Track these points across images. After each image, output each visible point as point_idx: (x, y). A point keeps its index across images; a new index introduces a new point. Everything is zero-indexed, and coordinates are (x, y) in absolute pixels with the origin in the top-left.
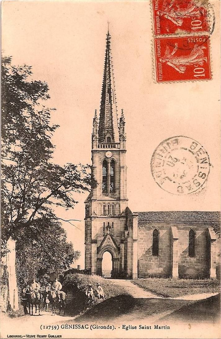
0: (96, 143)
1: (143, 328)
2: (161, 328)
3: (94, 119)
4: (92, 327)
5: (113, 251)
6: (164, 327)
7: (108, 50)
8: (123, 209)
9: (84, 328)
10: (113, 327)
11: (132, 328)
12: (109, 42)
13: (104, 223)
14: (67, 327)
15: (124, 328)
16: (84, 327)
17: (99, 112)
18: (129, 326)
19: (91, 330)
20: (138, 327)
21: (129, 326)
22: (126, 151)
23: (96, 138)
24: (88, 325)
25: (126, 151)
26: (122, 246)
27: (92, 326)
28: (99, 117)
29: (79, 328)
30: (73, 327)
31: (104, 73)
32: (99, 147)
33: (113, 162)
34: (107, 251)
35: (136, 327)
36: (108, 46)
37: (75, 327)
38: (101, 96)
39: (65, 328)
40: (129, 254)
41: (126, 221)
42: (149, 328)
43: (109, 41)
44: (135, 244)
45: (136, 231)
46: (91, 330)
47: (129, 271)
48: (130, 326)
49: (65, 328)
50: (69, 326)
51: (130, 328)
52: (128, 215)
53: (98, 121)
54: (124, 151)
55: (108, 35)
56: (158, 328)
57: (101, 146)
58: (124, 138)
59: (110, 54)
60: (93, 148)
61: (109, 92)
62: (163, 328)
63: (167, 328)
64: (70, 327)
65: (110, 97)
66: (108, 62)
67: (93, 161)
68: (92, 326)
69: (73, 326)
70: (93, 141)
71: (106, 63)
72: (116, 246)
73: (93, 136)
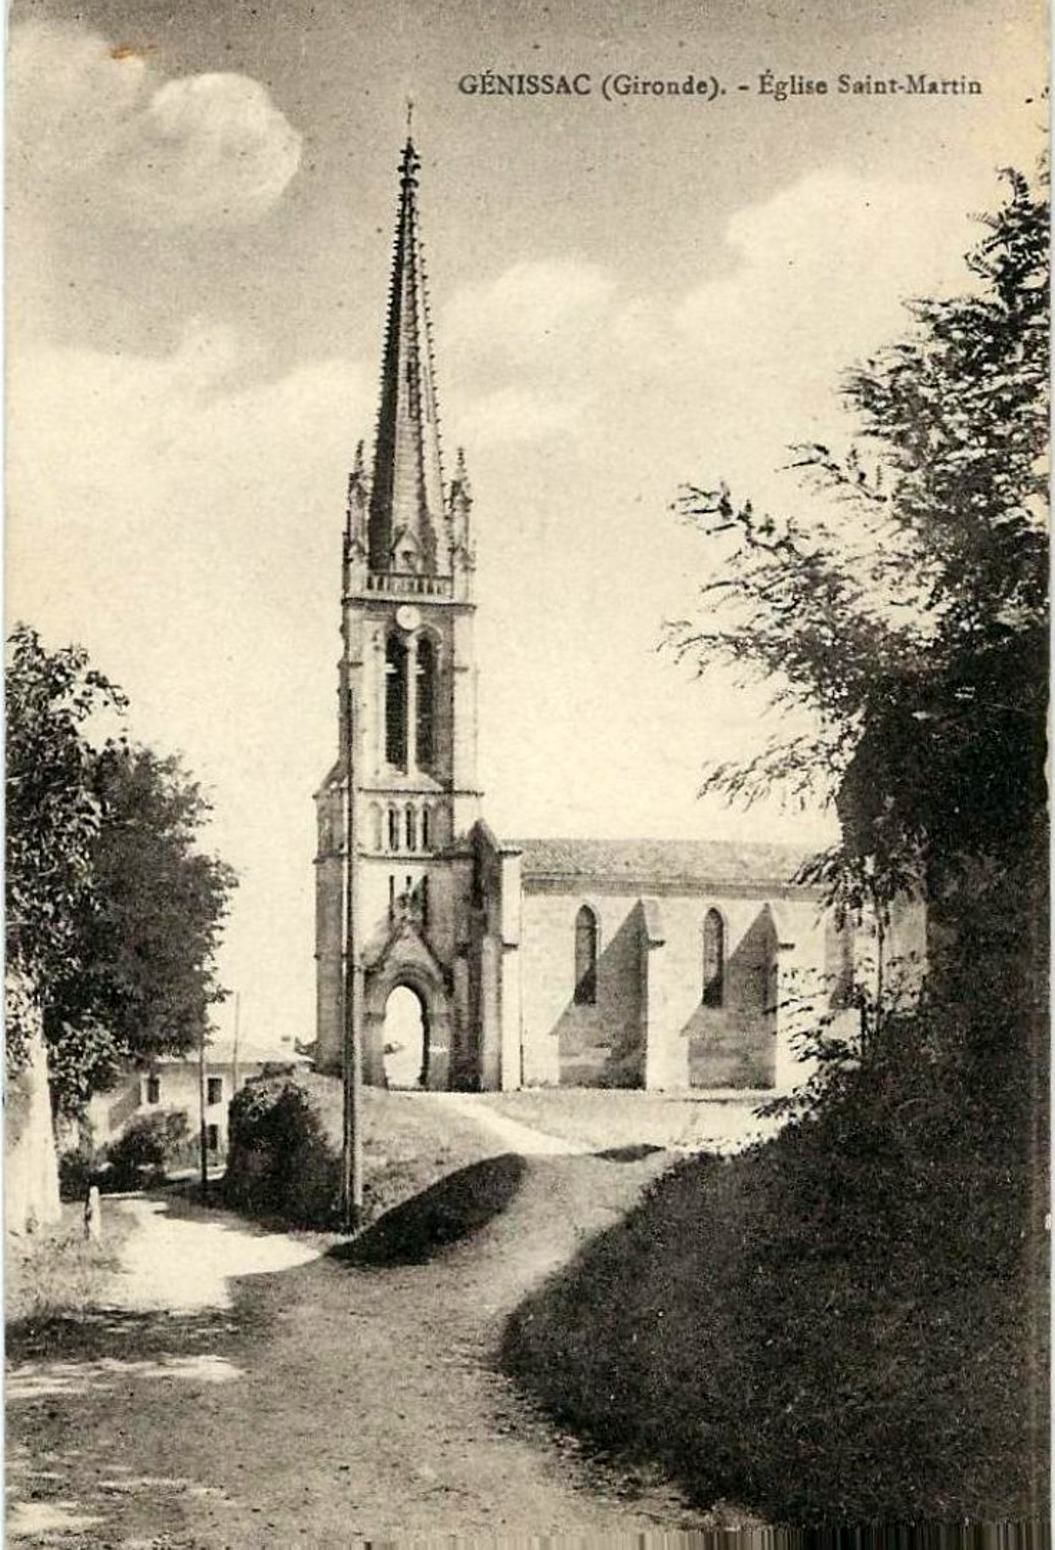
0: (359, 569)
1: (859, 88)
2: (940, 88)
3: (354, 477)
4: (610, 85)
5: (426, 987)
6: (955, 84)
7: (407, 212)
8: (463, 826)
9: (568, 91)
10: (710, 84)
11: (805, 88)
12: (412, 180)
13: (392, 879)
14: (490, 84)
15: (767, 88)
16: (572, 88)
17: (370, 452)
18: (793, 78)
19: (607, 98)
20: (833, 86)
21: (793, 78)
22: (475, 607)
23: (361, 550)
24: (587, 77)
25: (475, 607)
26: (460, 967)
27: (612, 81)
28: (369, 467)
29: (548, 88)
30: (516, 88)
31: (390, 301)
32: (370, 586)
33: (426, 646)
34: (400, 984)
35: (823, 84)
36: (406, 199)
37: (526, 85)
38: (383, 356)
39: (479, 89)
40: (489, 997)
41: (476, 872)
42: (888, 86)
43: (411, 176)
44: (509, 958)
45: (514, 906)
46: (607, 98)
47: (488, 1062)
48: (797, 80)
49: (479, 89)
50: (496, 80)
51: (797, 88)
52: (479, 858)
53: (368, 485)
54: (466, 608)
55: (409, 153)
56: (926, 88)
57: (381, 583)
58: (466, 557)
59: (415, 230)
60: (346, 588)
61: (412, 369)
62: (949, 88)
63: (967, 88)
64: (504, 89)
65: (415, 401)
66: (407, 258)
67: (346, 638)
68: (612, 81)
69: (516, 81)
70: (347, 561)
71: (399, 263)
72: (441, 966)
73: (348, 545)
